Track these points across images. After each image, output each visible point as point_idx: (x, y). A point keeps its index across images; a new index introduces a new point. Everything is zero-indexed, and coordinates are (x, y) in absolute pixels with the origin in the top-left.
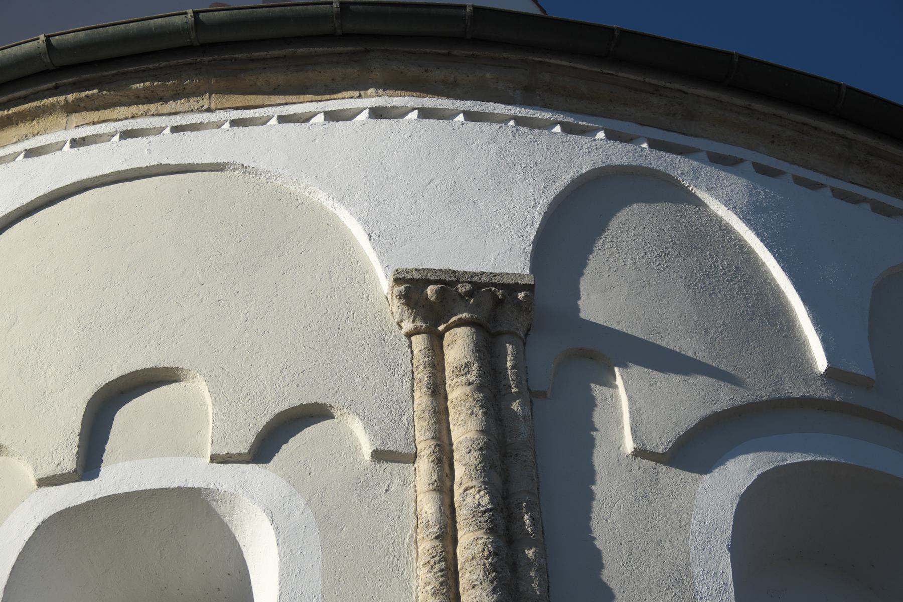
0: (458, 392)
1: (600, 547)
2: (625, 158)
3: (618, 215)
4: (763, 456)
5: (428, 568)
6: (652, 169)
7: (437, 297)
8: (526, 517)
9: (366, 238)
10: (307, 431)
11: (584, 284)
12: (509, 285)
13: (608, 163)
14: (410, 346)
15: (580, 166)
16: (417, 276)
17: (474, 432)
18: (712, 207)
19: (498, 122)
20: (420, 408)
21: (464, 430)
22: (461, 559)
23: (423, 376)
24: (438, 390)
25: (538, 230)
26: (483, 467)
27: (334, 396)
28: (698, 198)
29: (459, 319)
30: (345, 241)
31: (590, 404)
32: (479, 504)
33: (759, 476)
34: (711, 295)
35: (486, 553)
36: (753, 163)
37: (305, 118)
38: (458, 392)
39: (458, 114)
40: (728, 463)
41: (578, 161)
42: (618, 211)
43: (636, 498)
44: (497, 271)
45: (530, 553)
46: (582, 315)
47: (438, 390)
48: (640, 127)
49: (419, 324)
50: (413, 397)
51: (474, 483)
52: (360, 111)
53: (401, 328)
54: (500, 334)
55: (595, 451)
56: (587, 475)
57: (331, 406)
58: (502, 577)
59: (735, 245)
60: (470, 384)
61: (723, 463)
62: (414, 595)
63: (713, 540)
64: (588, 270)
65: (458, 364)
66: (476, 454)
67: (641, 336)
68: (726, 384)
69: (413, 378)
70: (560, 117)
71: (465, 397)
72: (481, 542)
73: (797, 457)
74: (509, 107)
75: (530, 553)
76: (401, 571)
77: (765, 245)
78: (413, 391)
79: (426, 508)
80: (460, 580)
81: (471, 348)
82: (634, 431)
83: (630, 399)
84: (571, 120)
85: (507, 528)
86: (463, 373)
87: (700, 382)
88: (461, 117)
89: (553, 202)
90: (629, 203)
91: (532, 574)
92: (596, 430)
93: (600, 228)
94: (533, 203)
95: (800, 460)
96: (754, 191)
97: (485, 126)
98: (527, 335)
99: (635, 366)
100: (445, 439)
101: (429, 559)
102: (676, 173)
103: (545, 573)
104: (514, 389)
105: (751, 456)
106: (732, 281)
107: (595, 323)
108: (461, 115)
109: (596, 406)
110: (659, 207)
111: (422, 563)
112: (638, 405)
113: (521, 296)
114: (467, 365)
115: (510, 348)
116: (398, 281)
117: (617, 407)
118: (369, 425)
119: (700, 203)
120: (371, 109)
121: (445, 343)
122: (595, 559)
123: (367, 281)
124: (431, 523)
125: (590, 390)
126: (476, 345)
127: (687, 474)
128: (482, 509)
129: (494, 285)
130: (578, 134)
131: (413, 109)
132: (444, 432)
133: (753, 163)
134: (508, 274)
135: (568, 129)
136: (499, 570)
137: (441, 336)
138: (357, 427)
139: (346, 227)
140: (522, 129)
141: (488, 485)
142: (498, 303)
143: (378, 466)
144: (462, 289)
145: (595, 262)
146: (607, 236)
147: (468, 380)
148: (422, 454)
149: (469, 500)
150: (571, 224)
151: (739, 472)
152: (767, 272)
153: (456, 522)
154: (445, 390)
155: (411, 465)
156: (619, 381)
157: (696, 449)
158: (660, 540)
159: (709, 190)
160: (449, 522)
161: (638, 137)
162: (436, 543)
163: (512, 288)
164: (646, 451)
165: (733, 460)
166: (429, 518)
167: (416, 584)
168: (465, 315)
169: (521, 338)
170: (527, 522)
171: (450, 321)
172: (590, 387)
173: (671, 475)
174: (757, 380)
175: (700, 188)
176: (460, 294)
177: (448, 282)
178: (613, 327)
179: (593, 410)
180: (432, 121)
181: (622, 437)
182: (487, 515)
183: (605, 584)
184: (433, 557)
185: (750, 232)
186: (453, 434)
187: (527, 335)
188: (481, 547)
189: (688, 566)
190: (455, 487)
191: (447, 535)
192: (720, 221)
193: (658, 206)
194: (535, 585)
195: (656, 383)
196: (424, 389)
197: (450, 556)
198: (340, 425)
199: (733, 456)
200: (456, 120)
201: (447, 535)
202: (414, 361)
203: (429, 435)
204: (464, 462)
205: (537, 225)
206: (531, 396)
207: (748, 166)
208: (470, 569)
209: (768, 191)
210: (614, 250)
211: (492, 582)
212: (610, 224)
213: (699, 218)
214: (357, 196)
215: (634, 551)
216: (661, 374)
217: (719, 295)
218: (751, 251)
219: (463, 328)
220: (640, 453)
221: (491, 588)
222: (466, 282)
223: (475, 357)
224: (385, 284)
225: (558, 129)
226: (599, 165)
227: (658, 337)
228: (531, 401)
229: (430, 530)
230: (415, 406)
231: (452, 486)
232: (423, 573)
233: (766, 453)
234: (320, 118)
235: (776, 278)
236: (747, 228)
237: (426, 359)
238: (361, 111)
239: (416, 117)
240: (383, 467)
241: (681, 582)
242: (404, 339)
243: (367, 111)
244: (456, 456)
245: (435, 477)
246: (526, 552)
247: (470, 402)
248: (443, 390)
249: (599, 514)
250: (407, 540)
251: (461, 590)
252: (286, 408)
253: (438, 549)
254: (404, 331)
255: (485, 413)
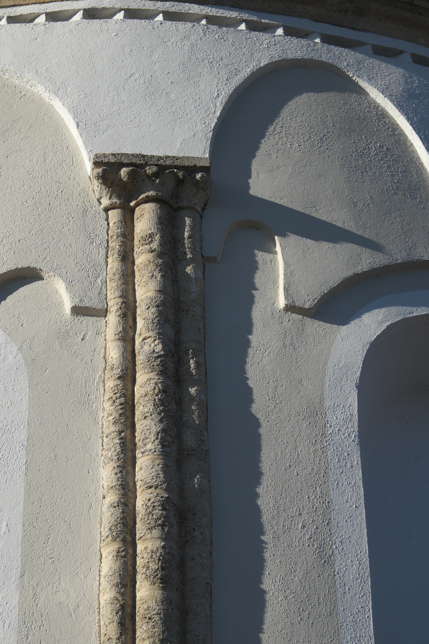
0: (142, 258)
1: (251, 386)
2: (299, 53)
3: (290, 103)
4: (394, 310)
5: (111, 402)
6: (322, 62)
7: (128, 178)
8: (191, 361)
9: (75, 126)
10: (21, 290)
11: (255, 165)
12: (189, 167)
13: (284, 57)
14: (107, 219)
15: (259, 61)
16: (112, 160)
17: (153, 292)
18: (371, 95)
19: (192, 22)
20: (112, 272)
21: (146, 290)
22: (137, 396)
23: (115, 245)
24: (127, 257)
25: (219, 118)
26: (159, 320)
27: (43, 261)
28: (360, 87)
29: (147, 196)
30: (59, 128)
31: (253, 267)
32: (154, 351)
33: (388, 327)
34: (362, 172)
35: (156, 391)
36: (412, 54)
37: (30, 19)
38: (142, 258)
39: (158, 14)
40: (363, 316)
41: (257, 55)
42: (290, 100)
43: (284, 346)
44: (181, 155)
45: (193, 390)
46: (252, 192)
47: (127, 257)
48: (315, 23)
49: (115, 200)
50: (107, 262)
51: (151, 334)
52: (75, 12)
53: (100, 203)
54: (180, 208)
55: (254, 307)
56: (245, 326)
57: (40, 270)
58: (168, 410)
59: (388, 129)
60: (152, 251)
61: (359, 316)
62: (100, 423)
63: (344, 379)
64: (259, 153)
65: (144, 234)
66: (153, 310)
67: (300, 210)
68: (368, 250)
69: (108, 246)
70: (245, 16)
71: (148, 263)
72: (153, 381)
73: (422, 311)
74: (202, 7)
75: (193, 390)
76: (91, 404)
77: (413, 128)
78: (107, 257)
79: (112, 355)
80: (136, 411)
81: (155, 221)
82: (286, 290)
83: (286, 263)
84: (255, 18)
85: (177, 371)
86: (147, 242)
87: (347, 249)
88: (160, 17)
89: (233, 93)
90: (299, 93)
91: (193, 408)
92: (256, 289)
93: (273, 115)
94: (216, 94)
95: (424, 313)
96: (409, 80)
97: (181, 25)
98: (204, 209)
99: (292, 235)
100: (131, 298)
101: (112, 395)
102: (342, 65)
103: (204, 407)
104: (189, 256)
105: (383, 310)
106: (382, 160)
107: (262, 199)
108: (161, 15)
109: (257, 269)
110: (325, 96)
111: (107, 398)
112: (292, 268)
113: (198, 176)
114: (151, 236)
115: (188, 221)
116: (96, 164)
117: (275, 270)
118: (70, 285)
119: (362, 92)
120: (85, 10)
121: (136, 217)
122: (247, 395)
123: (75, 163)
124: (115, 367)
125: (254, 255)
126: (159, 218)
127: (328, 325)
128: (155, 355)
129: (176, 167)
130: (259, 31)
131: (120, 10)
132: (131, 291)
133: (412, 54)
134: (188, 158)
135: (252, 27)
136: (166, 404)
137: (132, 210)
138: (61, 287)
139: (60, 117)
140: (212, 27)
141: (162, 336)
142: (180, 182)
143: (76, 319)
144: (149, 170)
145: (266, 145)
146: (279, 122)
147: (151, 248)
148: (111, 309)
149: (146, 348)
150: (246, 115)
151: (372, 324)
152: (414, 152)
153: (135, 365)
154: (133, 256)
155: (103, 318)
156: (278, 248)
157: (336, 305)
158: (301, 380)
159: (370, 80)
160: (130, 365)
161: (313, 33)
162: (118, 382)
163: (191, 170)
164: (295, 307)
165: (368, 314)
166: (114, 362)
167: (102, 415)
168: (151, 193)
169: (198, 212)
170: (192, 366)
171: (140, 198)
172: (254, 253)
173: (315, 326)
174: (395, 246)
175: (362, 78)
176: (148, 175)
177: (138, 165)
178: (276, 201)
179: (255, 273)
180: (135, 21)
181: (277, 295)
182: (159, 360)
183: (253, 415)
184: (115, 394)
185: (402, 117)
186: (137, 293)
187: (204, 209)
188: (153, 386)
189: (322, 401)
190: (136, 337)
191: (128, 376)
192: (377, 107)
193: (325, 95)
194: (195, 417)
195: (308, 249)
196: (116, 256)
197: (129, 393)
198: (48, 285)
199: (369, 310)
200: (156, 19)
201: (128, 376)
202: (109, 232)
203: (118, 294)
204: (144, 316)
205: (218, 114)
206: (204, 261)
207: (407, 58)
208: (143, 404)
209: (422, 79)
210: (283, 135)
211: (159, 414)
212: (282, 112)
213: (359, 105)
214: (69, 89)
215: (279, 388)
216: (313, 242)
217: (369, 173)
218: (402, 134)
219: (150, 204)
220: (290, 308)
221: (159, 418)
222: (153, 165)
223: (158, 229)
224: (88, 166)
225: (243, 27)
226: (276, 59)
227: (314, 210)
228: (204, 265)
229: (115, 372)
230: (108, 270)
231: (134, 336)
232: (107, 405)
233: (396, 307)
234: (42, 19)
235: (421, 157)
236: (399, 114)
237: (119, 231)
238: (77, 13)
239: (122, 18)
240: (81, 320)
241: (316, 413)
242: (103, 213)
243: (82, 12)
244: (138, 311)
245: (120, 329)
246: (190, 389)
247: (151, 267)
248: (131, 256)
249: (252, 358)
250: (97, 380)
251: (136, 420)
252: (4, 271)
253: (120, 387)
254: (102, 206)
255: (163, 276)
